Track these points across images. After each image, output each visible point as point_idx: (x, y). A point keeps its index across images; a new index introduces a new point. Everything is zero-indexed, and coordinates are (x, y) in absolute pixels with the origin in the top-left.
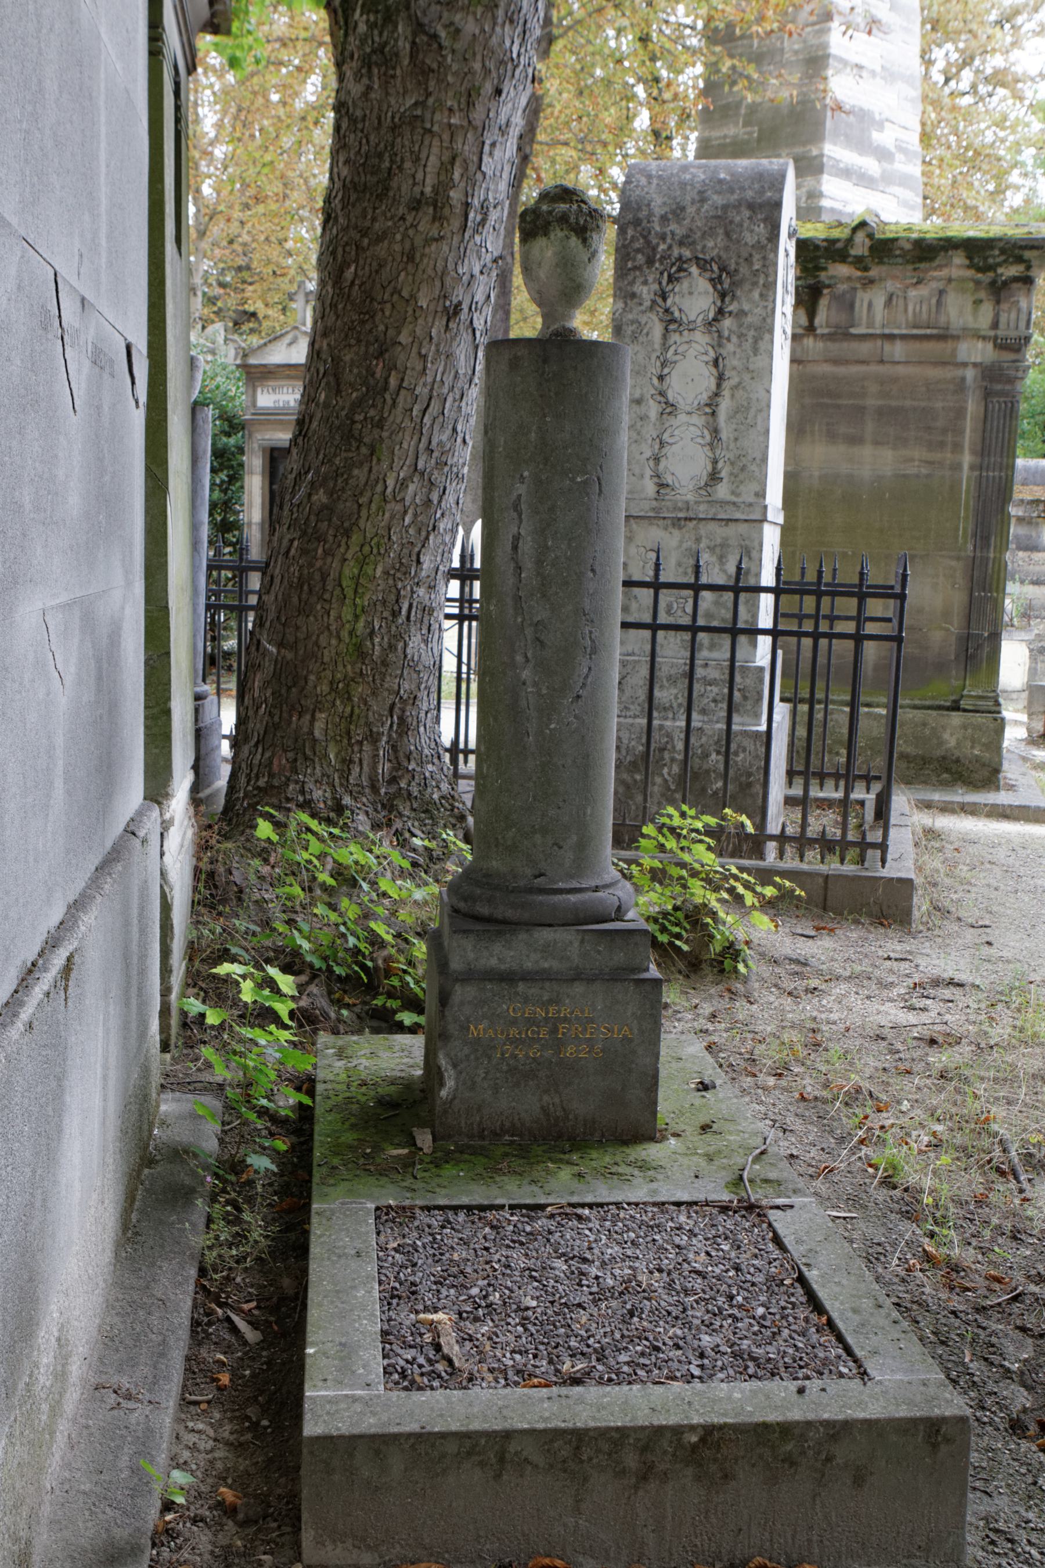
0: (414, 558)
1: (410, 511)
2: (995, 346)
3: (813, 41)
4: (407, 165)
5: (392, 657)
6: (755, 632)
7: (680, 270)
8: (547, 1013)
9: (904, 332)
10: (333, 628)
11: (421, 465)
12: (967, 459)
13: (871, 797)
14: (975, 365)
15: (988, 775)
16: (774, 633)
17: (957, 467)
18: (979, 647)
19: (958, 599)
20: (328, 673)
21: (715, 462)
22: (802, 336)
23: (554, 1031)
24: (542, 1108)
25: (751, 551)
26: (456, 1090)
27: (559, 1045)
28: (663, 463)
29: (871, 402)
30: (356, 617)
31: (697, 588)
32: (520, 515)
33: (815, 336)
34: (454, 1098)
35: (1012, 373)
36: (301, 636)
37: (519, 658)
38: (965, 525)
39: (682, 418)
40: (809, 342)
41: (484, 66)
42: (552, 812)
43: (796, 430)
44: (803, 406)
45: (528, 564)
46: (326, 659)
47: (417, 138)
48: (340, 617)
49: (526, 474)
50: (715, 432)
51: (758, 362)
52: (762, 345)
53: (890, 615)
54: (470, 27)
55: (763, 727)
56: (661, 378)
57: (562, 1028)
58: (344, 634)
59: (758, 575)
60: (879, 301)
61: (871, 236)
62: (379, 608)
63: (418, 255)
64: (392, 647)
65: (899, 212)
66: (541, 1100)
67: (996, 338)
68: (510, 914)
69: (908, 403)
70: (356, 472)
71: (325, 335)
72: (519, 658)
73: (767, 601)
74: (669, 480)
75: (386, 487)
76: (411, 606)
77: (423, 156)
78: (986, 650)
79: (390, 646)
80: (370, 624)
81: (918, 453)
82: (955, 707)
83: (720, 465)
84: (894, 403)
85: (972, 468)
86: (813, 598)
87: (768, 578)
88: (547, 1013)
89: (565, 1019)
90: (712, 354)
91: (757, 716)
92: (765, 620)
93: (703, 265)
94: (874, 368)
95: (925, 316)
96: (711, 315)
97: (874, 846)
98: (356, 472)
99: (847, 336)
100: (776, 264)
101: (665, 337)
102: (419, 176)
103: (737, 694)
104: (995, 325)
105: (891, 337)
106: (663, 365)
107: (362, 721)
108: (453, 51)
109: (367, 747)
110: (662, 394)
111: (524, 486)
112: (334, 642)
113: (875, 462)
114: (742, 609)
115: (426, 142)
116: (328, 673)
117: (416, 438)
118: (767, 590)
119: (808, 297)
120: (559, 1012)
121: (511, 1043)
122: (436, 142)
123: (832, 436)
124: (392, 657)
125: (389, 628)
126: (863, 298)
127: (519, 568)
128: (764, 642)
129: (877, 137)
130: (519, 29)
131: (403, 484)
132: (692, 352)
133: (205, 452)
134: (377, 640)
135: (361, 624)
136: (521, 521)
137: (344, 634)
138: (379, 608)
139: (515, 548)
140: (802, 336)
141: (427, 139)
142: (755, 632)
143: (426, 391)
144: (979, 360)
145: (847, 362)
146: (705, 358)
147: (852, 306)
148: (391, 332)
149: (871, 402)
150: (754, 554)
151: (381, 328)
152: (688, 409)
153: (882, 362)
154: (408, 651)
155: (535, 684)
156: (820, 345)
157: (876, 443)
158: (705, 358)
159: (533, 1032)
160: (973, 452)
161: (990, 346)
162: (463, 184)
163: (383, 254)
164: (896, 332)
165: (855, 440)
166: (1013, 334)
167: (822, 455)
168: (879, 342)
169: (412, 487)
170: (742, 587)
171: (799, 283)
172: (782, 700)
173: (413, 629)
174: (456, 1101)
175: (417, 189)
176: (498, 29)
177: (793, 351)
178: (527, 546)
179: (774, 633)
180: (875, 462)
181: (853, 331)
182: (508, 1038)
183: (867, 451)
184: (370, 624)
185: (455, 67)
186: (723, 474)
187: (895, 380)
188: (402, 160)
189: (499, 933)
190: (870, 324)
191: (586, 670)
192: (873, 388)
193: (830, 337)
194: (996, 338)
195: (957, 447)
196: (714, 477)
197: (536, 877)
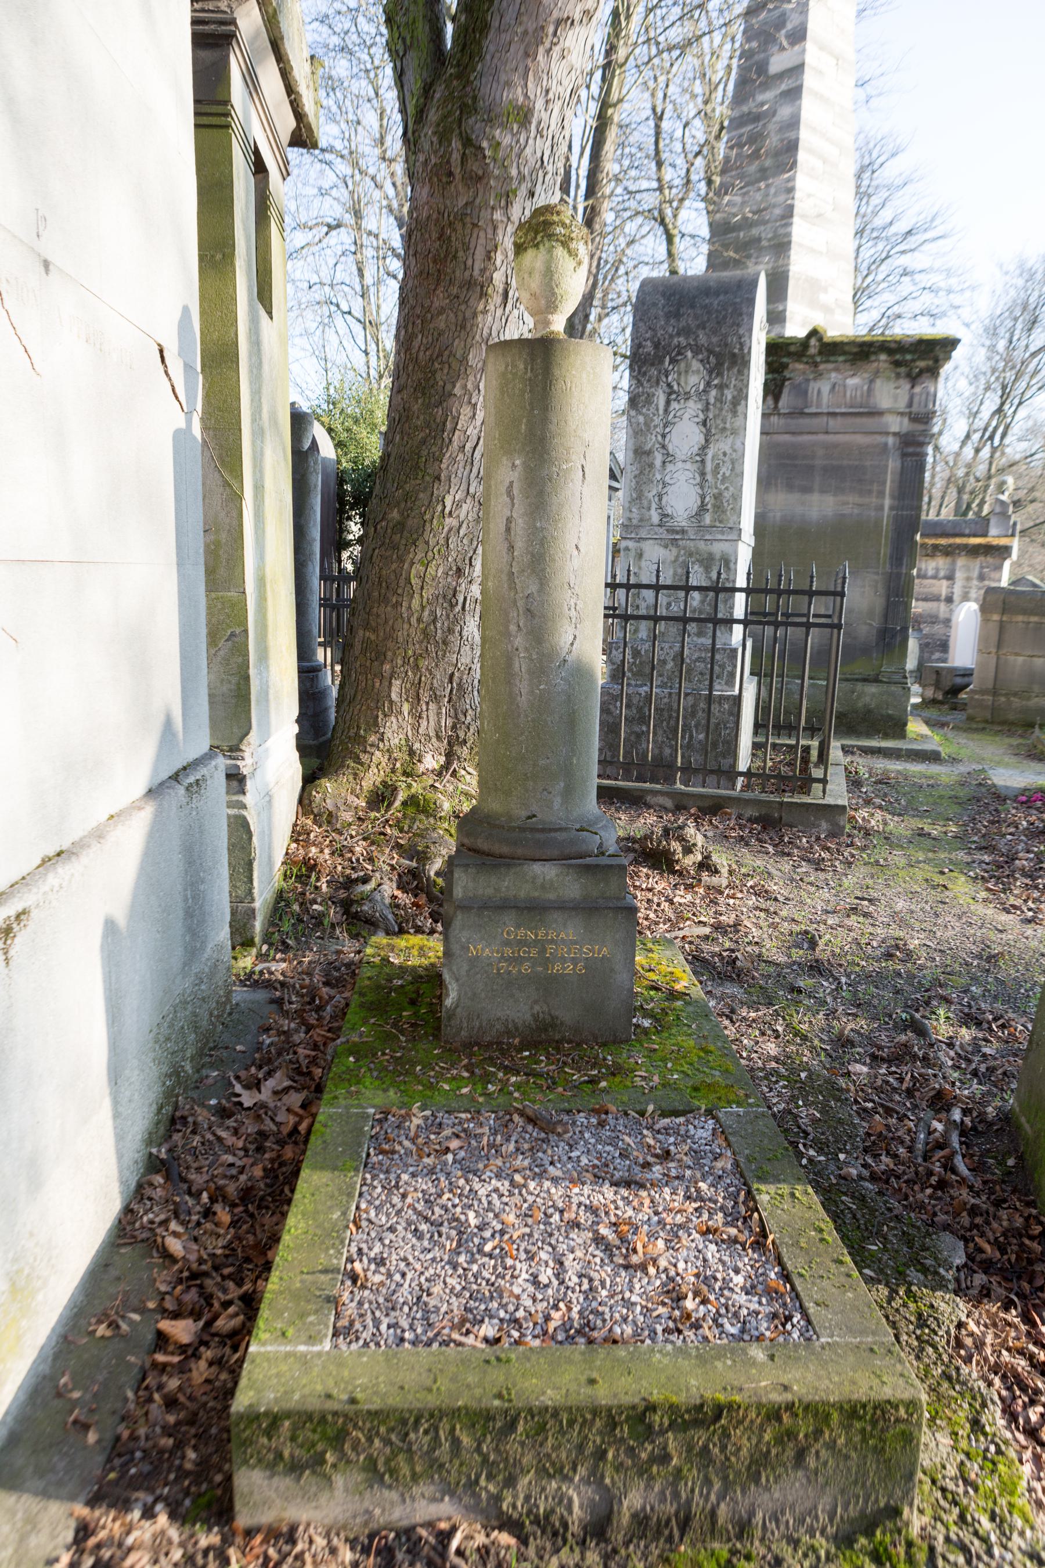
0: (467, 561)
1: (464, 526)
2: (910, 419)
3: (782, 231)
4: (461, 254)
5: (451, 638)
6: (731, 621)
7: (679, 353)
8: (536, 936)
9: (843, 410)
10: (405, 615)
11: (472, 490)
12: (887, 502)
13: (815, 743)
14: (895, 434)
15: (898, 728)
16: (745, 622)
17: (881, 508)
18: (894, 636)
19: (879, 603)
20: (401, 650)
21: (703, 497)
22: (770, 414)
23: (543, 950)
24: (533, 1015)
25: (728, 562)
26: (459, 999)
27: (546, 962)
28: (665, 498)
29: (819, 462)
30: (423, 608)
31: (688, 589)
32: (512, 500)
33: (779, 414)
34: (457, 1006)
35: (921, 439)
36: (381, 621)
37: (513, 628)
38: (885, 550)
39: (680, 465)
40: (774, 419)
41: (519, 173)
42: (541, 762)
43: (765, 482)
44: (769, 466)
45: (520, 545)
46: (401, 640)
47: (468, 231)
48: (410, 607)
49: (517, 462)
50: (703, 474)
51: (738, 422)
52: (740, 409)
53: (830, 612)
54: (507, 140)
55: (737, 692)
56: (664, 436)
57: (551, 948)
58: (414, 621)
59: (734, 581)
60: (826, 388)
61: (820, 339)
62: (441, 601)
63: (468, 325)
64: (450, 631)
65: (843, 325)
66: (532, 1008)
67: (910, 413)
68: (505, 850)
69: (845, 462)
70: (421, 495)
71: (399, 392)
72: (513, 628)
73: (740, 599)
74: (669, 511)
75: (445, 507)
76: (465, 599)
77: (472, 246)
78: (898, 639)
79: (449, 630)
80: (433, 613)
81: (852, 498)
82: (876, 680)
83: (707, 499)
84: (835, 463)
85: (891, 508)
86: (772, 628)
87: (741, 582)
88: (536, 936)
89: (552, 941)
90: (702, 416)
91: (733, 686)
92: (739, 612)
93: (697, 350)
94: (821, 437)
95: (859, 399)
96: (702, 387)
97: (818, 781)
98: (421, 495)
99: (802, 414)
100: (751, 316)
101: (668, 403)
102: (469, 262)
103: (716, 668)
104: (910, 404)
105: (834, 414)
106: (665, 427)
107: (428, 687)
108: (495, 160)
109: (432, 706)
110: (664, 447)
111: (516, 474)
112: (406, 626)
113: (820, 506)
114: (721, 606)
115: (475, 235)
116: (401, 650)
117: (468, 468)
118: (741, 590)
119: (773, 390)
120: (547, 934)
121: (506, 961)
122: (482, 234)
123: (790, 487)
124: (451, 638)
125: (448, 616)
126: (814, 387)
127: (511, 548)
128: (738, 630)
129: (823, 297)
130: (549, 143)
131: (458, 505)
132: (686, 416)
133: (316, 486)
134: (439, 625)
135: (426, 613)
136: (513, 505)
137: (414, 621)
138: (441, 601)
139: (508, 530)
140: (770, 414)
141: (476, 231)
142: (731, 621)
143: (476, 431)
144: (897, 430)
145: (801, 433)
146: (697, 420)
147: (806, 392)
148: (448, 387)
149: (819, 462)
150: (732, 565)
151: (441, 383)
152: (684, 458)
153: (827, 433)
154: (465, 633)
155: (526, 649)
156: (782, 421)
157: (822, 491)
158: (697, 420)
159: (525, 952)
160: (892, 497)
161: (906, 420)
162: (503, 268)
163: (442, 326)
164: (838, 410)
165: (806, 490)
166: (923, 410)
167: (784, 502)
168: (825, 419)
169: (465, 507)
170: (722, 590)
171: (770, 376)
172: (752, 674)
173: (467, 618)
174: (459, 1010)
175: (467, 274)
176: (531, 141)
177: (763, 426)
178: (520, 524)
179: (745, 622)
180: (820, 506)
181: (806, 411)
182: (502, 957)
183: (815, 497)
184: (433, 613)
185: (496, 172)
186: (709, 506)
187: (835, 446)
188: (457, 251)
189: (495, 866)
190: (819, 405)
191: (571, 638)
192: (820, 452)
193: (790, 415)
194: (910, 413)
195: (881, 494)
196: (702, 508)
197: (529, 818)
